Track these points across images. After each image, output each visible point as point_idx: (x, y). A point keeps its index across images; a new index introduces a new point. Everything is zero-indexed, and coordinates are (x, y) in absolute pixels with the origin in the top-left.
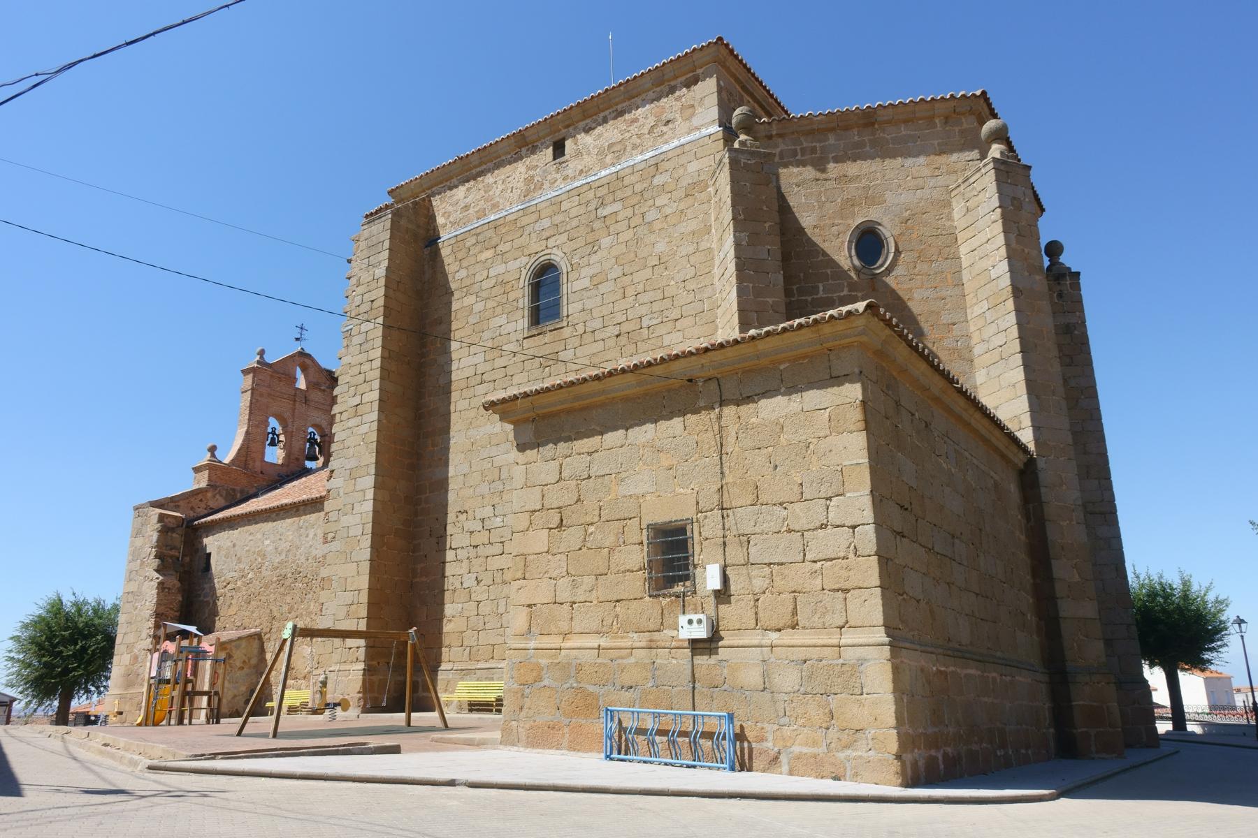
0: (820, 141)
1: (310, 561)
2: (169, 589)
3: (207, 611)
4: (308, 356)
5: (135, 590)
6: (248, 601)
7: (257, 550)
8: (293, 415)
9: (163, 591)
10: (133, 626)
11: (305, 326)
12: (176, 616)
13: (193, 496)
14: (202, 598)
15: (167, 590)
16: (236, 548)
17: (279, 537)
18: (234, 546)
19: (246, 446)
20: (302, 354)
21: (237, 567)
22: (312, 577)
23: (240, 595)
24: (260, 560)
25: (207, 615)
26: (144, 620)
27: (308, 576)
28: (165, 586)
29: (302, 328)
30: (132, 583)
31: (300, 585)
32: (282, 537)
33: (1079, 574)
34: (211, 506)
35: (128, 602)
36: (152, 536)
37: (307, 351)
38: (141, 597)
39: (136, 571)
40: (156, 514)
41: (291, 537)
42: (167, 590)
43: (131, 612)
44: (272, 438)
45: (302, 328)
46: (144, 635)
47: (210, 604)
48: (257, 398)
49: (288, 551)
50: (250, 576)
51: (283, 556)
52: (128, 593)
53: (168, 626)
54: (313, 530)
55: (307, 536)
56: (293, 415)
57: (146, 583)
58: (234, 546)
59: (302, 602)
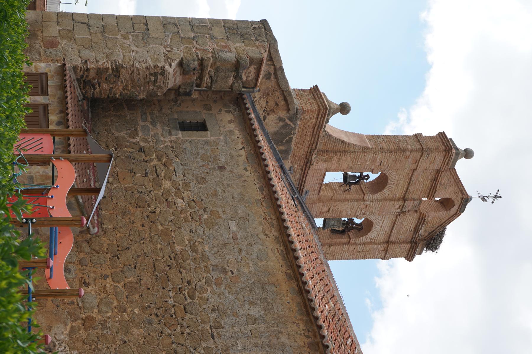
0: (207, 67)
1: (213, 315)
2: (155, 82)
3: (122, 134)
4: (462, 209)
5: (152, 34)
6: (141, 204)
7: (220, 210)
8: (385, 199)
9: (151, 74)
10: (100, 36)
11: (497, 201)
12: (115, 94)
13: (283, 94)
14: (141, 123)
15: (153, 79)
16: (218, 172)
17: (244, 248)
18: (222, 168)
19: (347, 149)
20: (466, 200)
21: (190, 177)
22: (185, 324)
23: (150, 187)
24: (205, 216)
25: (117, 134)
26: (107, 51)
27: (188, 315)
28: (159, 77)
29: (496, 197)
30: (161, 27)
31: (171, 302)
32: (243, 254)
33: (112, 279)
34: (268, 117)
35: (133, 24)
36: (230, 51)
37: (469, 206)
38: (142, 44)
39: (178, 33)
40: (261, 54)
41: (246, 271)
42: (153, 79)
43: (119, 31)
44: (355, 176)
45: (496, 197)
46: (87, 54)
47: (133, 138)
48: (411, 156)
49: (224, 271)
50: (179, 201)
51: (214, 261)
52: (146, 24)
53: (107, 163)
54: (262, 313)
55: (251, 303)
56: (385, 199)
57: (162, 49)
58: (222, 168)
59: (144, 309)
